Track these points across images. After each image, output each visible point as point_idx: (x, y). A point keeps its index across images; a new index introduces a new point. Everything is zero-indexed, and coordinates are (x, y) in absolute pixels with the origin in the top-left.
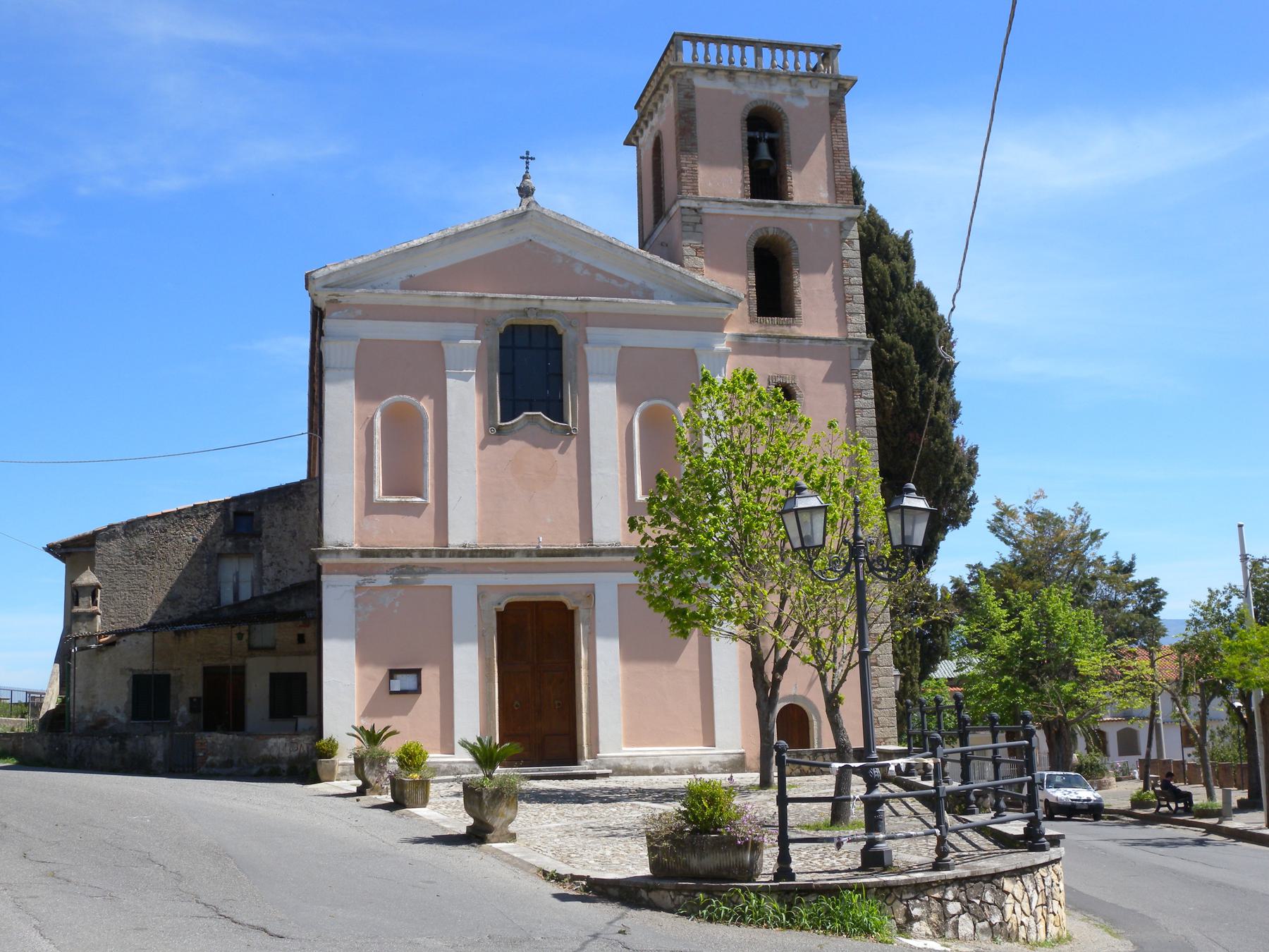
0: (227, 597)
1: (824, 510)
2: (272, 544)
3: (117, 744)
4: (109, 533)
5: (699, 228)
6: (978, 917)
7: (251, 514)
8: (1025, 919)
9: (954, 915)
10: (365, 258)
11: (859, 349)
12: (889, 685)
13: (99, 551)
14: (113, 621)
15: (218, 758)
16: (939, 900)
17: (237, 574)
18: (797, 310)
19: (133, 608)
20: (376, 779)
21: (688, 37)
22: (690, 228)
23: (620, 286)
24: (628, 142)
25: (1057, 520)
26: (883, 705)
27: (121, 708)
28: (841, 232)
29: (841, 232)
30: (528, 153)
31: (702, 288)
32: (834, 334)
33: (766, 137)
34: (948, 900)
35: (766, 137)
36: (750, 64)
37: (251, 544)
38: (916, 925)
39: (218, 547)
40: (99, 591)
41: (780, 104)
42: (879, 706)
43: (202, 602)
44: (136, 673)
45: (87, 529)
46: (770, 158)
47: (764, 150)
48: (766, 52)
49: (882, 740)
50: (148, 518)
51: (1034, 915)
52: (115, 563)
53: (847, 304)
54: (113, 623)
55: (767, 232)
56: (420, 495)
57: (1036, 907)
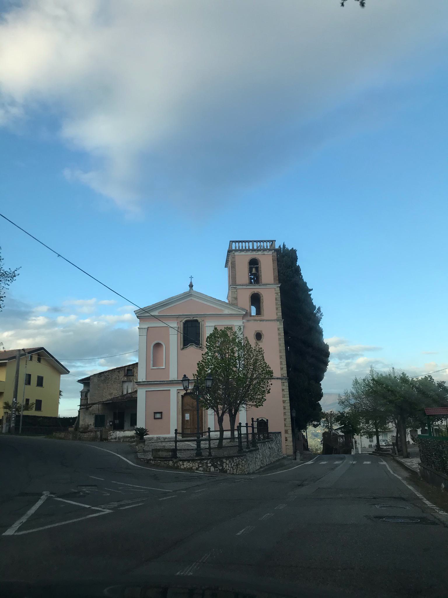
0: (125, 393)
9: (209, 467)
17: (127, 387)
21: (233, 242)
24: (225, 267)
25: (269, 371)
34: (208, 463)
37: (131, 378)
38: (200, 468)
44: (96, 415)
47: (254, 271)
51: (233, 468)
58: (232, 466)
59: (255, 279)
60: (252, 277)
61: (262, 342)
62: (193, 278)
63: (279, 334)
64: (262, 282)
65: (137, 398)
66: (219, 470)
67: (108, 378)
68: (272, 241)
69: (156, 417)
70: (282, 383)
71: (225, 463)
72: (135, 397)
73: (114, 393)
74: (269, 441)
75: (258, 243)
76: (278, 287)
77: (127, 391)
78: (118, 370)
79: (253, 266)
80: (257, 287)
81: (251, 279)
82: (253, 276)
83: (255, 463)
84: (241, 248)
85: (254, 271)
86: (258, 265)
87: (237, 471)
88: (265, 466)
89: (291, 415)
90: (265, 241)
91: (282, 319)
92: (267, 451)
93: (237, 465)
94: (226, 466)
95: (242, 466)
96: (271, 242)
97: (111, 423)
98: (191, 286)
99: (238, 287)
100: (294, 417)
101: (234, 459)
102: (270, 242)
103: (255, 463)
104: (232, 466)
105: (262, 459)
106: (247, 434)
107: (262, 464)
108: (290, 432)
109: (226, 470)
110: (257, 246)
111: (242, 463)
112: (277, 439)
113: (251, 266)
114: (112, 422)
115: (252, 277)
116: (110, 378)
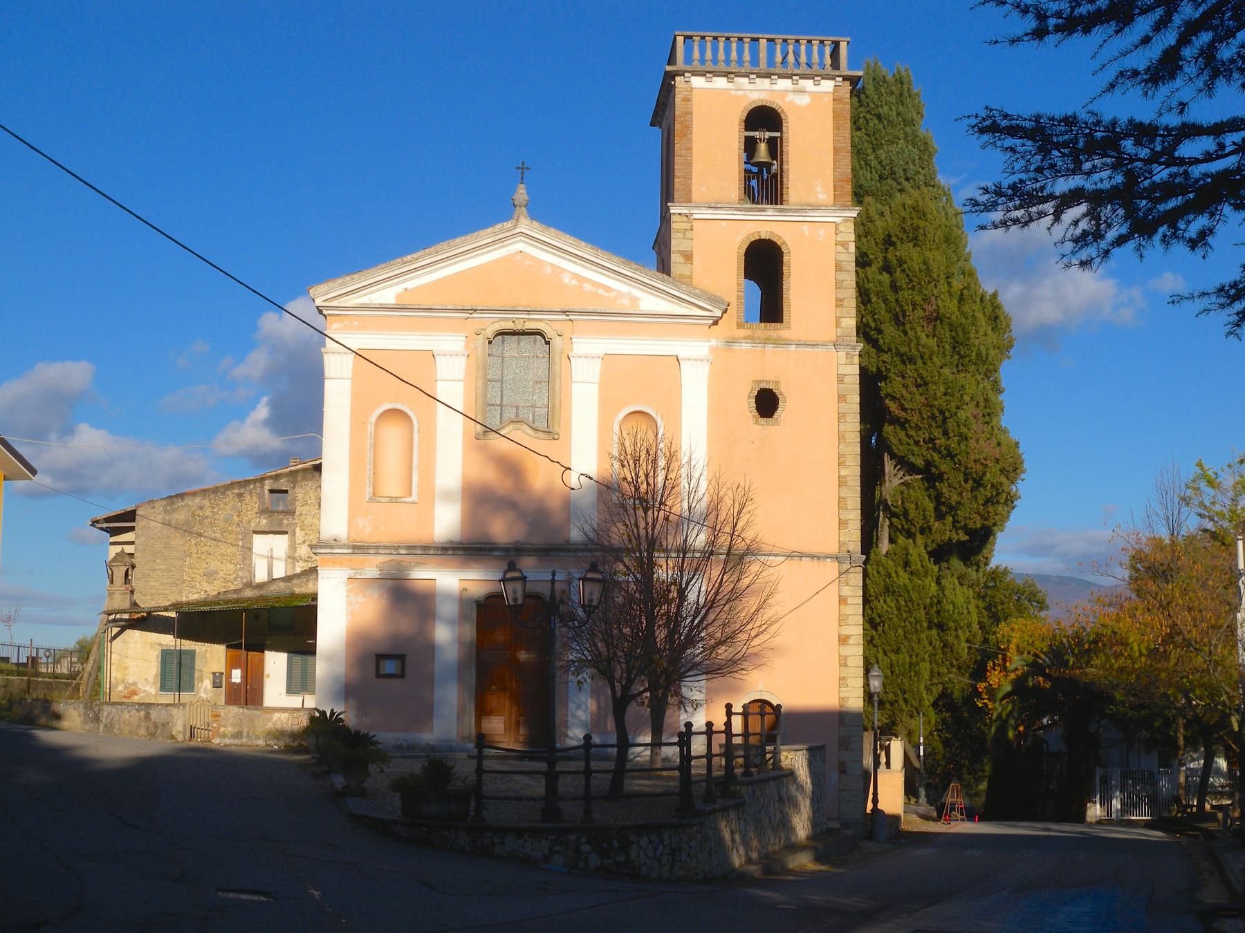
2: (306, 522)
3: (142, 713)
5: (689, 234)
7: (286, 492)
15: (230, 729)
20: (1205, 648)
23: (607, 295)
24: (652, 124)
27: (151, 679)
30: (523, 163)
33: (766, 137)
38: (556, 856)
39: (253, 524)
41: (781, 103)
43: (236, 578)
44: (164, 648)
62: (527, 169)
63: (842, 398)
65: (314, 597)
67: (199, 516)
69: (382, 672)
71: (635, 845)
72: (305, 596)
73: (221, 574)
76: (846, 220)
77: (270, 572)
78: (236, 491)
79: (757, 133)
80: (770, 212)
89: (867, 685)
94: (638, 855)
106: (709, 755)
111: (691, 847)
113: (751, 134)
116: (207, 517)
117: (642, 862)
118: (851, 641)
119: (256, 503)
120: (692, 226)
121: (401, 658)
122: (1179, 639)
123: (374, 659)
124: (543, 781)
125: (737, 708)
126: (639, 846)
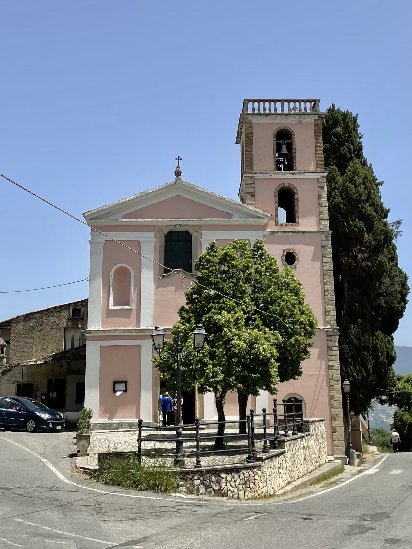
0: (69, 347)
1: (162, 336)
4: (17, 320)
5: (253, 185)
6: (207, 487)
8: (231, 489)
9: (197, 485)
10: (107, 206)
11: (325, 235)
12: (339, 389)
13: (12, 328)
14: (18, 359)
16: (191, 479)
17: (73, 336)
18: (297, 219)
19: (27, 353)
22: (249, 186)
24: (237, 143)
26: (335, 398)
28: (318, 183)
29: (318, 183)
31: (252, 212)
32: (315, 229)
33: (285, 143)
35: (285, 143)
36: (279, 111)
40: (5, 348)
42: (333, 399)
44: (18, 383)
45: (8, 319)
46: (287, 152)
47: (284, 150)
48: (286, 104)
49: (335, 415)
50: (34, 313)
52: (19, 333)
53: (320, 216)
54: (18, 360)
55: (284, 185)
56: (129, 306)
57: (239, 484)
58: (237, 484)
59: (286, 163)
60: (281, 160)
61: (295, 268)
62: (181, 159)
64: (297, 168)
66: (213, 492)
68: (315, 101)
69: (124, 384)
70: (327, 336)
71: (225, 479)
74: (304, 437)
75: (292, 103)
79: (281, 141)
80: (289, 175)
81: (279, 163)
82: (282, 159)
83: (278, 477)
84: (262, 111)
85: (284, 150)
86: (290, 140)
87: (245, 493)
88: (296, 479)
90: (303, 100)
91: (329, 231)
92: (301, 454)
93: (245, 483)
94: (226, 485)
95: (254, 484)
96: (313, 103)
97: (43, 398)
98: (178, 174)
99: (257, 176)
100: (348, 393)
101: (241, 473)
102: (311, 102)
103: (278, 477)
104: (237, 484)
105: (290, 468)
107: (290, 477)
108: (341, 417)
109: (226, 492)
110: (289, 108)
111: (255, 479)
112: (317, 432)
113: (279, 141)
114: (45, 395)
115: (281, 160)
117: (229, 490)
118: (335, 368)
119: (66, 315)
120: (254, 182)
121: (126, 382)
122: (144, 524)
123: (112, 383)
124: (175, 443)
125: (279, 401)
126: (226, 480)
